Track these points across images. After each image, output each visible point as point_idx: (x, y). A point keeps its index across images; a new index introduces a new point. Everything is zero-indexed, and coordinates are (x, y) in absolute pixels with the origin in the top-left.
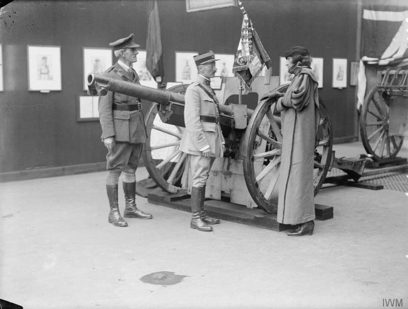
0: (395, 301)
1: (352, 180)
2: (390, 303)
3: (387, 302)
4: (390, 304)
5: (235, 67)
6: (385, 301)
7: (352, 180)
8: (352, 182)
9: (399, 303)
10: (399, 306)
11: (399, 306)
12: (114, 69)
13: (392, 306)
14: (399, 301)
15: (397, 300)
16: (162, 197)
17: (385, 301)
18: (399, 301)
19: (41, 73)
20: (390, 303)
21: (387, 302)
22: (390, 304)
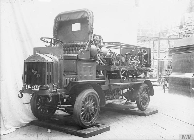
0: (188, 136)
1: (47, 111)
2: (185, 137)
3: (184, 137)
4: (185, 138)
5: (115, 98)
6: (183, 136)
7: (47, 111)
8: (47, 111)
9: (190, 137)
10: (190, 138)
11: (190, 138)
12: (167, 32)
13: (187, 138)
14: (190, 136)
15: (189, 136)
16: (108, 90)
17: (183, 136)
18: (190, 136)
19: (153, 41)
20: (185, 137)
21: (184, 137)
22: (185, 138)
